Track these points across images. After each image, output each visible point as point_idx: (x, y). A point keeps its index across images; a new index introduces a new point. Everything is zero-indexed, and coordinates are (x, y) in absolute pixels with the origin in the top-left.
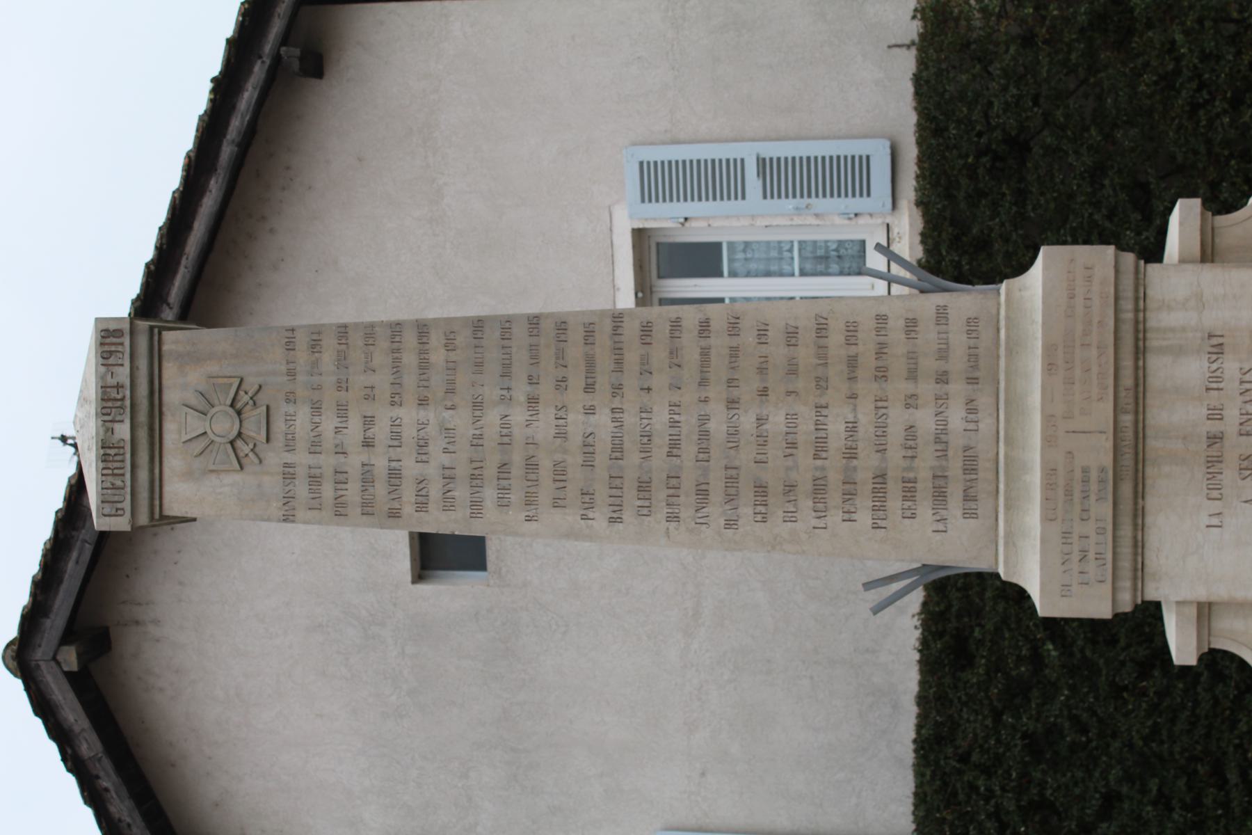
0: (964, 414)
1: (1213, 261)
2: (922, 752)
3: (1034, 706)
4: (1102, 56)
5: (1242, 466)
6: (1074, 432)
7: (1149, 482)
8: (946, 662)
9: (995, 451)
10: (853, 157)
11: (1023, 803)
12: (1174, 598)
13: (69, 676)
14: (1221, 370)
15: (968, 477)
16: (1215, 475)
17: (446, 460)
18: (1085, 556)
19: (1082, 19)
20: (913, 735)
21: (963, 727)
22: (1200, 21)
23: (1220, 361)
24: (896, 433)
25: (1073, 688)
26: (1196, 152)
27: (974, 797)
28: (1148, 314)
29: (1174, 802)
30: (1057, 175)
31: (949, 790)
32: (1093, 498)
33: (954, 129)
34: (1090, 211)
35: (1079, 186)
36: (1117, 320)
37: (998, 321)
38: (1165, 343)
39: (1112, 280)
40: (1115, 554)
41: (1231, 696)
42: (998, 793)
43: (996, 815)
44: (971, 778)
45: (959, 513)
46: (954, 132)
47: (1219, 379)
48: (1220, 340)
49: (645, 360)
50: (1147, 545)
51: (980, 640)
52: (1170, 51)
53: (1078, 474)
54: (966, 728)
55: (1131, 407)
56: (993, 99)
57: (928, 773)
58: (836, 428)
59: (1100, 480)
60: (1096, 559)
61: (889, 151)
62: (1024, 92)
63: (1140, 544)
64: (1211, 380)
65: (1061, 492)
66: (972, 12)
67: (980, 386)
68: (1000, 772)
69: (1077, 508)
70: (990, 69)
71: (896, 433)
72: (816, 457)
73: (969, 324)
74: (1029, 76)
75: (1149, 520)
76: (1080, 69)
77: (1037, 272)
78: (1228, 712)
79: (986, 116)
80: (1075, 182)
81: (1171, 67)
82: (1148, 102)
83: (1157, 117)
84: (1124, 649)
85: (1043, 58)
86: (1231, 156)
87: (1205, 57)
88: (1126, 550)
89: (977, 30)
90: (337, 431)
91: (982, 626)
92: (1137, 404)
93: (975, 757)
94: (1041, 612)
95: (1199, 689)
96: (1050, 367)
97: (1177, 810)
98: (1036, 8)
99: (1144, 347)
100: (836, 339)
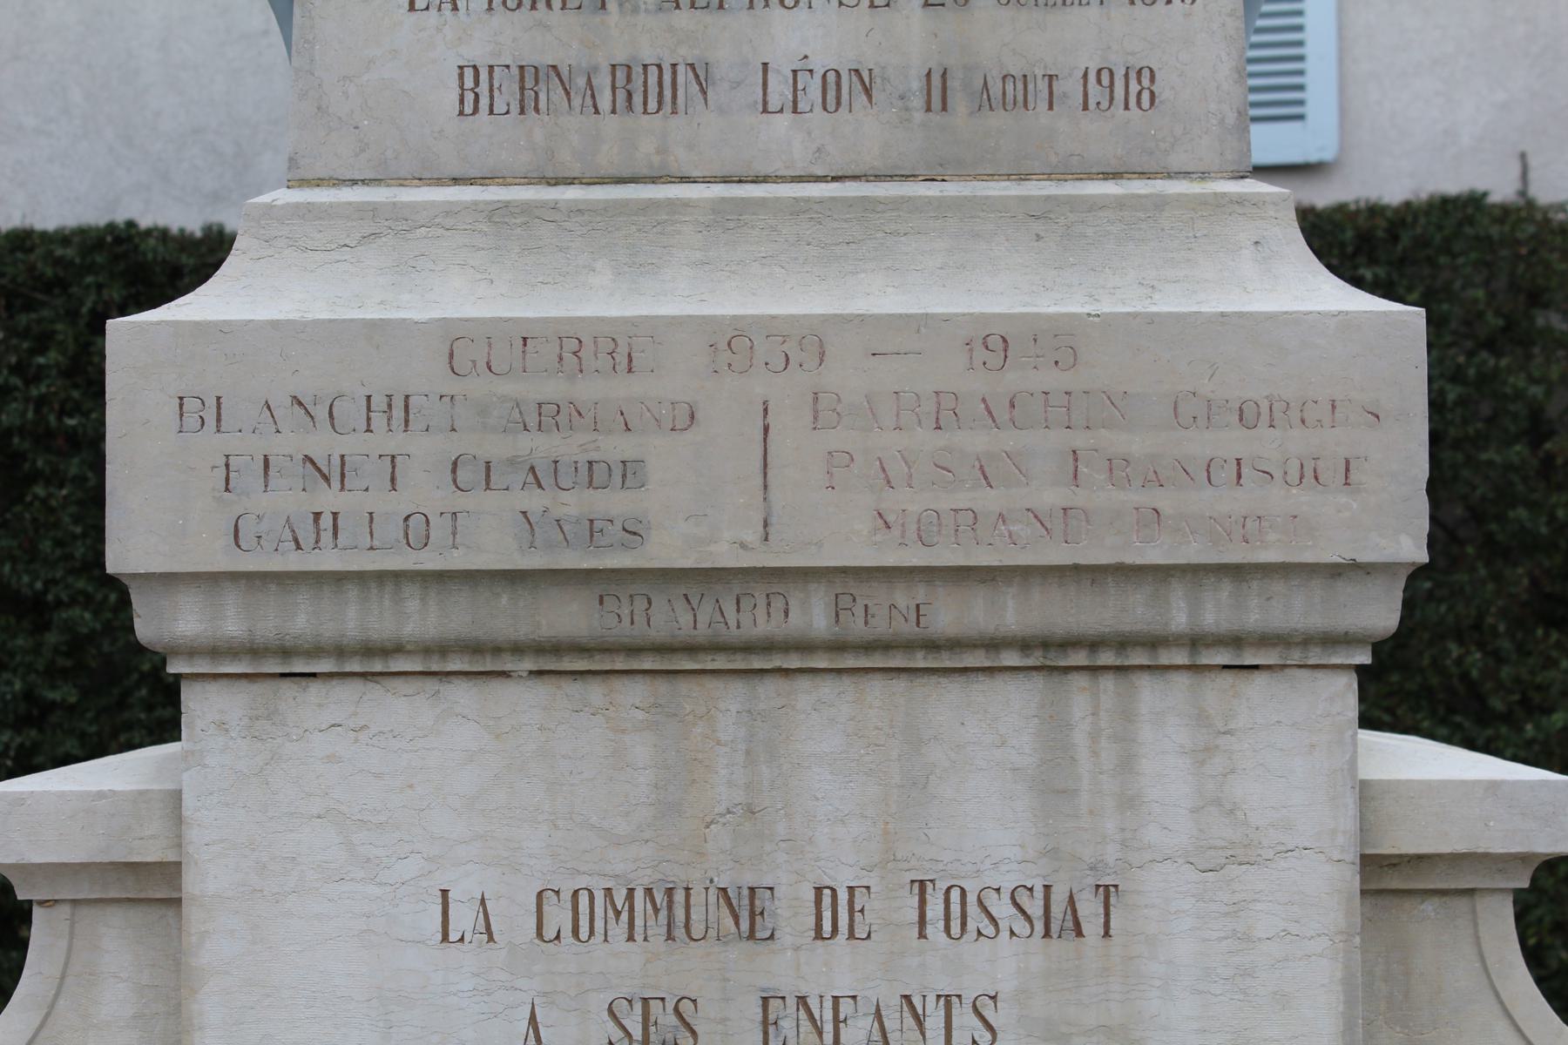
0: (819, 64)
1: (1363, 892)
2: (109, 239)
5: (655, 1006)
6: (766, 429)
7: (595, 692)
9: (695, 173)
10: (1301, 88)
11: (16, 440)
12: (190, 784)
14: (990, 931)
15: (603, 81)
16: (625, 916)
18: (326, 479)
20: (145, 222)
23: (1021, 927)
27: (25, 345)
28: (1182, 680)
29: (33, 733)
31: (40, 296)
32: (534, 501)
37: (1144, 175)
38: (1080, 737)
39: (1308, 557)
40: (339, 579)
42: (34, 392)
44: (60, 337)
45: (477, 52)
47: (956, 925)
48: (1093, 927)
50: (374, 690)
52: (1525, 702)
53: (616, 447)
55: (856, 627)
57: (70, 252)
59: (598, 525)
60: (317, 516)
61: (1313, 157)
64: (955, 895)
65: (553, 389)
67: (919, 116)
68: (76, 394)
69: (496, 447)
73: (1133, 75)
75: (462, 695)
81: (1497, 704)
82: (1426, 661)
92: (869, 647)
94: (116, 327)
96: (995, 342)
97: (18, 740)
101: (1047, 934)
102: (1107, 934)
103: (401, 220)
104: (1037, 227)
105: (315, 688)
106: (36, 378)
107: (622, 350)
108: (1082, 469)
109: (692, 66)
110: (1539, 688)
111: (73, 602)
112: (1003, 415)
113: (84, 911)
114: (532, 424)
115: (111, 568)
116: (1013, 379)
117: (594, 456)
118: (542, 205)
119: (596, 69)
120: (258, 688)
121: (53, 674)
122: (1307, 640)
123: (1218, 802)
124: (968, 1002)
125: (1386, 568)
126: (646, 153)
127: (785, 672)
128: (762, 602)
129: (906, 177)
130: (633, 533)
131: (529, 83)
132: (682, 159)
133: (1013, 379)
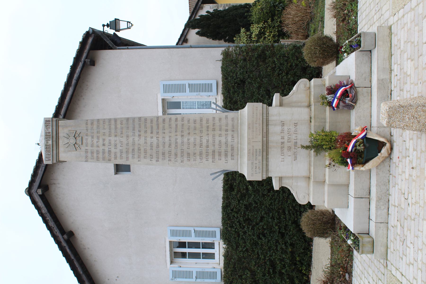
13: (40, 196)
15: (232, 151)
17: (121, 148)
19: (256, 56)
22: (280, 57)
24: (217, 142)
25: (254, 195)
26: (279, 84)
28: (269, 117)
32: (258, 155)
35: (255, 90)
36: (263, 118)
37: (238, 118)
40: (262, 167)
45: (230, 159)
47: (283, 131)
48: (284, 123)
49: (164, 127)
52: (274, 63)
53: (255, 151)
55: (266, 136)
57: (225, 213)
58: (204, 141)
65: (251, 154)
68: (240, 213)
69: (255, 158)
71: (217, 142)
72: (200, 147)
78: (286, 199)
79: (236, 75)
81: (274, 66)
86: (286, 84)
87: (281, 64)
88: (265, 166)
90: (97, 142)
91: (236, 183)
93: (234, 210)
98: (247, 53)
100: (204, 122)
105: (269, 169)
106: (237, 217)
110: (272, 61)
111: (261, 214)
121: (269, 216)
122: (267, 110)
125: (262, 105)
129: (238, 133)
130: (260, 150)
132: (237, 146)
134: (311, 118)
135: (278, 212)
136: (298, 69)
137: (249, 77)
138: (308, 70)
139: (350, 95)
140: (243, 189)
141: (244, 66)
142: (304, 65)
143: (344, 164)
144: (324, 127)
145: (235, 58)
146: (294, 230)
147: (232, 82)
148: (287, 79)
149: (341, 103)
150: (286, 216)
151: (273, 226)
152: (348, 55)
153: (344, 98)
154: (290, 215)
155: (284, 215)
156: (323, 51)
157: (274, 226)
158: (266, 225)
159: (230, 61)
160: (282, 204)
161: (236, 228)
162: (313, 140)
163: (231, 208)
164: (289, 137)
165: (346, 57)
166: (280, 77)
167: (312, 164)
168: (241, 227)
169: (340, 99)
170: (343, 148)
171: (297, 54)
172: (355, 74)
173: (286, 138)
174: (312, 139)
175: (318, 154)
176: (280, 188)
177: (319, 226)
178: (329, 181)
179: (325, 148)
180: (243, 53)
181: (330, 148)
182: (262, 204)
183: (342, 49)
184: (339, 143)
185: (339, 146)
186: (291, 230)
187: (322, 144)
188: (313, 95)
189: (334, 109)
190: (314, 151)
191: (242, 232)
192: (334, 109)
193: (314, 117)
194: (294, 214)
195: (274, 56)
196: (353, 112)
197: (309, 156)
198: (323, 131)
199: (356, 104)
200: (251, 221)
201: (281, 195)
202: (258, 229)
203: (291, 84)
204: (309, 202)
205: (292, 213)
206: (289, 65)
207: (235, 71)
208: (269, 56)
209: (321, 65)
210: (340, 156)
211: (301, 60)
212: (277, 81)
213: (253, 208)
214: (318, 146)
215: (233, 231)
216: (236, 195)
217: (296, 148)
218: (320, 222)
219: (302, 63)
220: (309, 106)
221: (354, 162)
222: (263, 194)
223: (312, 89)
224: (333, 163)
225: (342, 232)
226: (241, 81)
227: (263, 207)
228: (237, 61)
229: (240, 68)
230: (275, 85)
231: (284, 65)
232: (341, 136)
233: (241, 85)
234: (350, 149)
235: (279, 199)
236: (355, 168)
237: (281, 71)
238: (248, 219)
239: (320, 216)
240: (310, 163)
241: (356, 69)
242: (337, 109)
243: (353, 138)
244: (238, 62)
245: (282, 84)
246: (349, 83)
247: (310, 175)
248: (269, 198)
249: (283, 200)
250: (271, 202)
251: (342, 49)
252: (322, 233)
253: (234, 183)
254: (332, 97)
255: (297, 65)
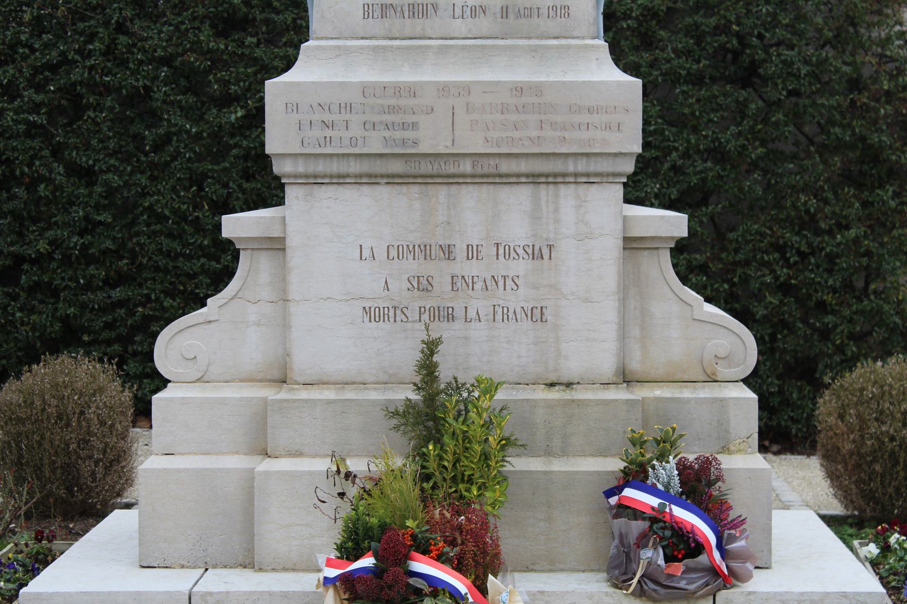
0: (470, 4)
1: (624, 248)
3: (178, 98)
4: (836, 159)
5: (421, 279)
6: (453, 114)
7: (404, 189)
8: (220, 9)
9: (433, 37)
15: (406, 9)
16: (412, 253)
18: (328, 127)
19: (875, 138)
21: (153, 27)
22: (868, 253)
23: (526, 256)
25: (198, 137)
26: (736, 251)
28: (572, 186)
30: (718, 115)
31: (88, 13)
32: (387, 134)
33: (767, 10)
34: (680, 148)
35: (706, 137)
36: (567, 155)
38: (543, 203)
40: (331, 155)
41: (197, 291)
43: (65, 62)
46: (764, 10)
48: (546, 257)
50: (341, 188)
51: (243, 43)
53: (410, 119)
54: (152, 30)
55: (479, 170)
56: (796, 49)
60: (325, 138)
62: (802, 81)
63: (342, 181)
64: (507, 247)
65: (392, 102)
66: (887, 28)
67: (499, 20)
68: (109, 65)
69: (376, 118)
70: (828, 48)
74: (818, 86)
75: (366, 189)
76: (824, 137)
77: (618, 76)
78: (182, 288)
79: (779, 44)
80: (710, 133)
81: (823, 225)
83: (773, 213)
84: (240, 186)
85: (837, 100)
86: (733, 285)
87: (831, 258)
88: (335, 167)
89: (868, 34)
91: (258, 45)
92: (483, 176)
93: (123, 39)
95: (203, 260)
96: (519, 89)
98: (888, 93)
99: (539, 183)
101: (533, 258)
102: (550, 259)
103: (347, 50)
104: (533, 54)
105: (323, 187)
106: (90, 54)
107: (412, 91)
108: (543, 125)
109: (432, 4)
110: (845, 217)
111: (108, 170)
112: (521, 110)
113: (255, 252)
114: (387, 112)
115: (267, 152)
116: (524, 100)
117: (404, 121)
118: (389, 46)
119: (404, 5)
120: (308, 187)
121: (98, 208)
122: (608, 175)
123: (582, 221)
124: (510, 278)
126: (418, 31)
127: (459, 183)
128: (452, 163)
130: (415, 143)
131: (384, 9)
132: (429, 32)
133: (524, 100)
134: (569, 385)
135: (117, 252)
136: (806, 342)
137: (773, 105)
138: (800, 390)
139: (678, 568)
140: (229, 82)
141: (827, 83)
142: (826, 366)
143: (349, 538)
144: (525, 449)
145: (865, 38)
146: (34, 329)
147: (749, 22)
148: (760, 290)
149: (637, 526)
150: (101, 289)
151: (49, 228)
152: (868, 564)
153: (662, 539)
154: (103, 310)
155: (106, 282)
156: (890, 456)
157: (50, 234)
158: (53, 193)
159: (851, 13)
160: (157, 269)
161: (33, 50)
162: (465, 395)
163: (132, 20)
164: (479, 285)
165: (862, 555)
166: (766, 252)
167: (350, 394)
168: (36, 71)
169: (660, 521)
170: (428, 535)
171: (879, 334)
172: (778, 589)
173: (472, 269)
174: (470, 393)
175: (395, 421)
176: (230, 242)
177: (51, 442)
178: (267, 473)
179: (424, 450)
180: (891, 77)
181: (427, 477)
182: (156, 173)
183: (896, 535)
184: (448, 515)
185: (437, 516)
186: (34, 317)
187: (446, 439)
188: (677, 395)
189: (609, 493)
190: (410, 400)
191: (13, 75)
192: (609, 493)
193: (573, 401)
194: (109, 326)
195: (870, 227)
196: (598, 581)
197: (385, 378)
198: (506, 443)
199: (632, 594)
200: (70, 124)
201: (203, 265)
202: (33, 157)
203: (737, 306)
204: (163, 383)
205: (115, 320)
206: (828, 298)
207: (800, 34)
208: (872, 204)
209: (823, 446)
210: (388, 521)
211: (849, 353)
212: (747, 242)
213: (134, 129)
214: (435, 419)
215: (19, 32)
216: (196, 47)
217: (425, 317)
218: (73, 446)
219: (837, 359)
220: (626, 378)
221: (360, 588)
222: (204, 176)
223: (705, 392)
224: (353, 491)
225: (27, 545)
226: (753, 67)
227: (143, 181)
228: (850, 47)
229: (814, 59)
230: (733, 229)
231: (825, 275)
232: (485, 526)
233: (732, 69)
234: (421, 566)
235: (183, 255)
236: (331, 592)
237: (797, 259)
238: (77, 108)
239: (101, 446)
240: (353, 383)
241: (802, 594)
242: (611, 508)
243: (474, 583)
244: (844, 51)
245: (736, 263)
246: (734, 565)
247: (299, 384)
248: (185, 207)
249: (177, 276)
250: (167, 218)
251: (900, 533)
252: (21, 457)
253: (257, 34)
254: (669, 483)
255: (825, 334)
